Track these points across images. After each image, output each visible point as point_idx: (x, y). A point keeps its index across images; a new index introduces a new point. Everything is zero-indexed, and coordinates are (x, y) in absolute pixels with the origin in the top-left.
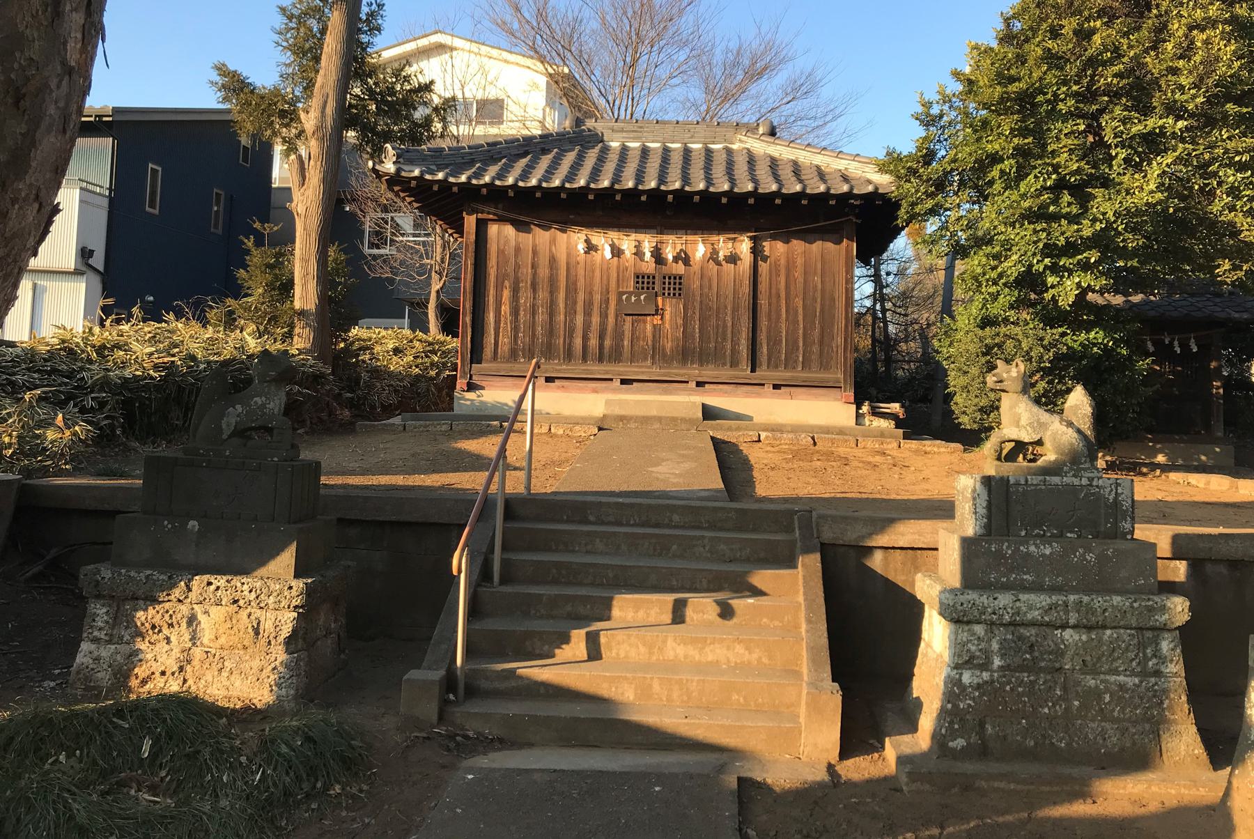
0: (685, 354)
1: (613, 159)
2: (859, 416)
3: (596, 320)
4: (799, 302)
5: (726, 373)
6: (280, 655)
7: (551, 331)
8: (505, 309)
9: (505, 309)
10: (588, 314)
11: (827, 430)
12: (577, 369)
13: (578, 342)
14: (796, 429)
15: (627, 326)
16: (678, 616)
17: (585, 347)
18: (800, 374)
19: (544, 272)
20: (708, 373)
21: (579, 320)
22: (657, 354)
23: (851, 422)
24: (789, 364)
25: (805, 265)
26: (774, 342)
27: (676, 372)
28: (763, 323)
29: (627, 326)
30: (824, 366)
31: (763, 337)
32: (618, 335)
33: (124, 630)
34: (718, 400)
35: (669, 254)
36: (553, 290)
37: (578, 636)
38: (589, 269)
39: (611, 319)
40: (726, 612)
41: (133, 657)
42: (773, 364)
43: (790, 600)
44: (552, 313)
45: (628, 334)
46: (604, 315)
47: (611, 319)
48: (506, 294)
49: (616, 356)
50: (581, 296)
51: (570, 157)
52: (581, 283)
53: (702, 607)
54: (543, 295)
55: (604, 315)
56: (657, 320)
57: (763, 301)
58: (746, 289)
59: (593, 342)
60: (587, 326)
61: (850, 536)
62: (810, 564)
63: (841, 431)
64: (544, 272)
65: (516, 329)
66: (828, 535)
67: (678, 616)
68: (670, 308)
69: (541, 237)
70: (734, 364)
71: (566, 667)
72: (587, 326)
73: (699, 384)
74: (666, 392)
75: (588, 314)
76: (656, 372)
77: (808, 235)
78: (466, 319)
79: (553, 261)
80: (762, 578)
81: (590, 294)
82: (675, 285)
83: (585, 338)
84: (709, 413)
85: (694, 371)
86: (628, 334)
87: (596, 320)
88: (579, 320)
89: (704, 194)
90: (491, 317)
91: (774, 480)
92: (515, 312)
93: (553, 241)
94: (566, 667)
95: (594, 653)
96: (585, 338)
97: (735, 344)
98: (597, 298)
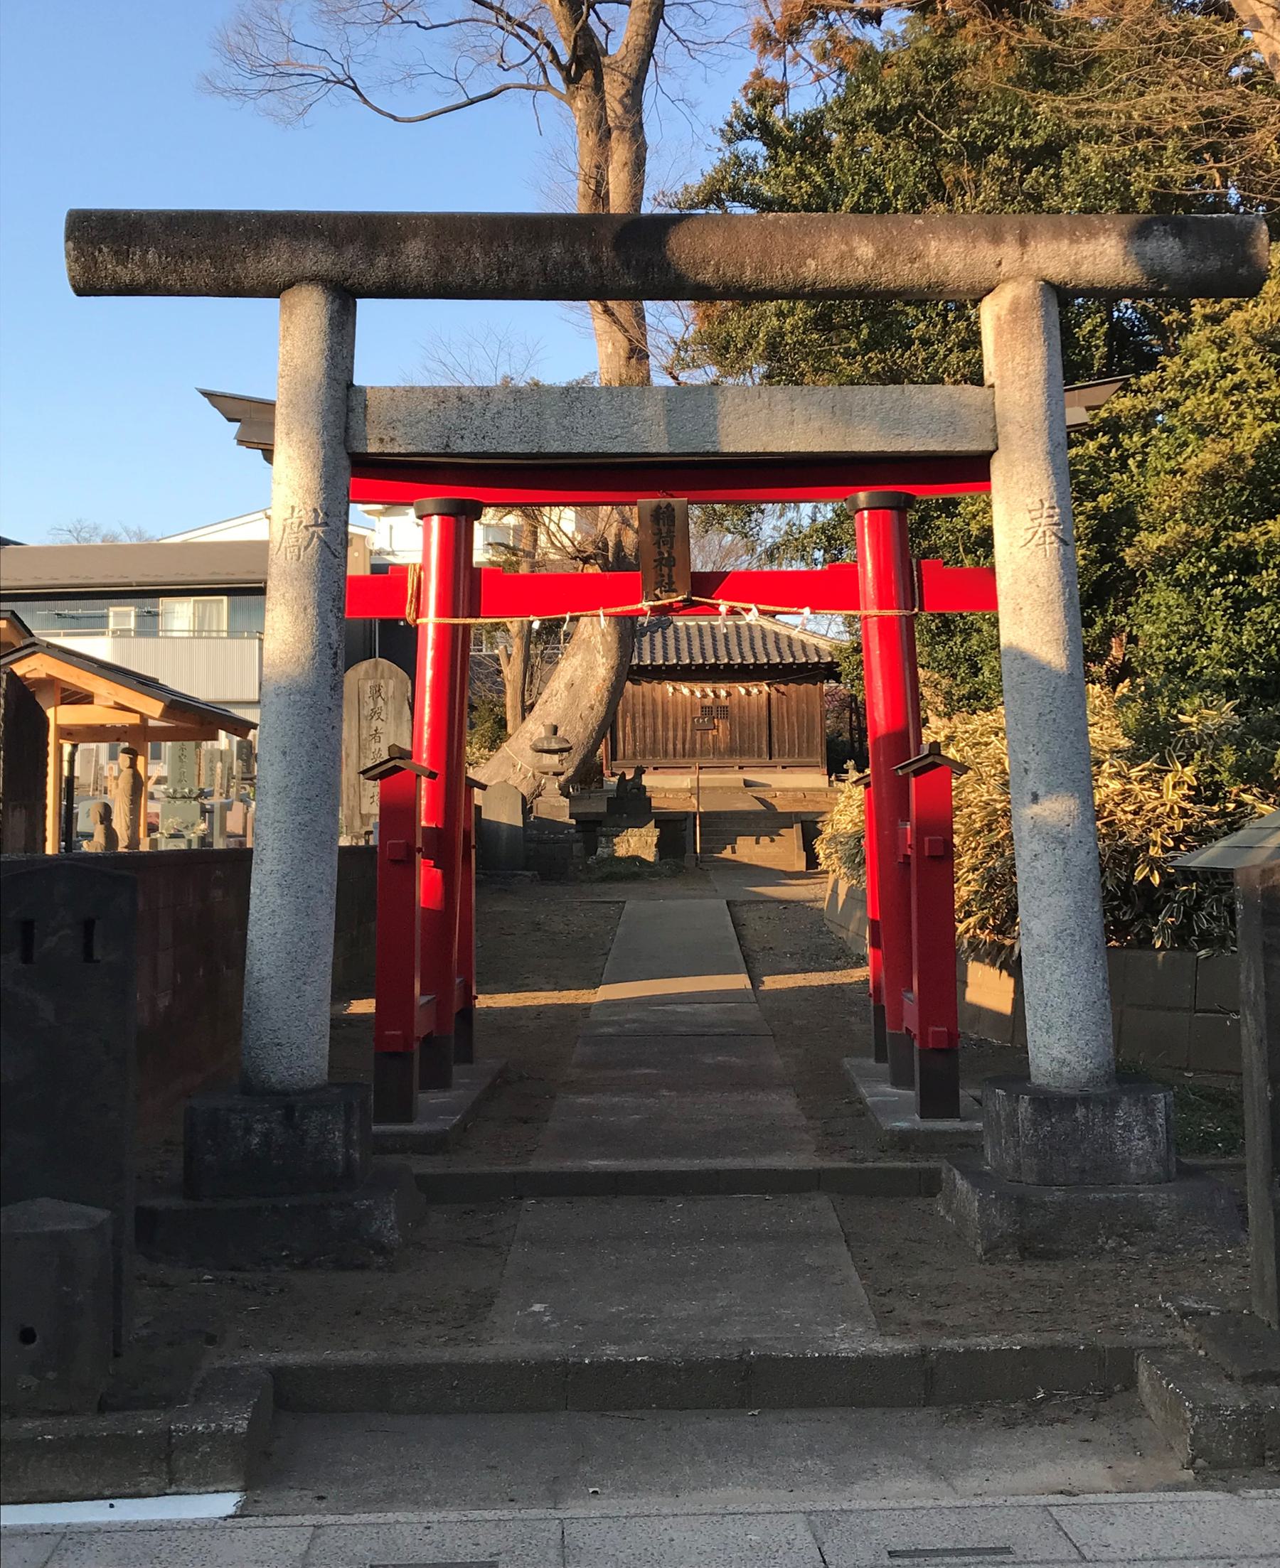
0: (732, 751)
1: (683, 635)
2: (830, 782)
3: (680, 733)
4: (795, 719)
5: (755, 761)
6: (654, 849)
7: (655, 741)
8: (628, 729)
9: (628, 729)
10: (675, 730)
11: (812, 790)
12: (672, 762)
13: (671, 746)
14: (795, 790)
15: (698, 737)
16: (757, 842)
17: (675, 749)
18: (797, 760)
19: (649, 708)
20: (745, 761)
21: (671, 734)
22: (716, 752)
23: (827, 785)
24: (791, 754)
25: (797, 696)
26: (781, 742)
27: (727, 761)
28: (775, 732)
29: (698, 737)
30: (809, 754)
31: (775, 739)
32: (693, 742)
33: (610, 844)
34: (751, 777)
35: (723, 693)
36: (655, 718)
37: (729, 847)
38: (675, 703)
39: (689, 733)
40: (772, 840)
41: (614, 851)
42: (781, 755)
43: (793, 836)
44: (655, 731)
45: (698, 741)
46: (685, 730)
47: (689, 733)
48: (628, 720)
49: (693, 754)
50: (671, 721)
51: (658, 636)
52: (671, 713)
53: (765, 840)
54: (649, 721)
55: (685, 730)
56: (715, 732)
57: (774, 719)
58: (765, 712)
59: (679, 746)
60: (675, 738)
61: (810, 818)
62: (798, 827)
63: (819, 790)
64: (649, 708)
65: (635, 741)
66: (803, 818)
67: (757, 842)
68: (722, 725)
69: (646, 687)
70: (760, 756)
71: (727, 853)
72: (675, 738)
73: (741, 768)
74: (722, 773)
75: (675, 730)
76: (716, 762)
77: (798, 682)
78: (466, 706)
79: (654, 700)
80: (782, 831)
81: (676, 719)
82: (724, 712)
83: (675, 745)
84: (747, 784)
85: (738, 761)
86: (698, 741)
87: (680, 733)
88: (671, 734)
89: (740, 665)
90: (621, 734)
91: (782, 806)
92: (634, 731)
93: (653, 689)
94: (727, 853)
95: (734, 852)
96: (675, 745)
97: (760, 743)
98: (680, 721)
